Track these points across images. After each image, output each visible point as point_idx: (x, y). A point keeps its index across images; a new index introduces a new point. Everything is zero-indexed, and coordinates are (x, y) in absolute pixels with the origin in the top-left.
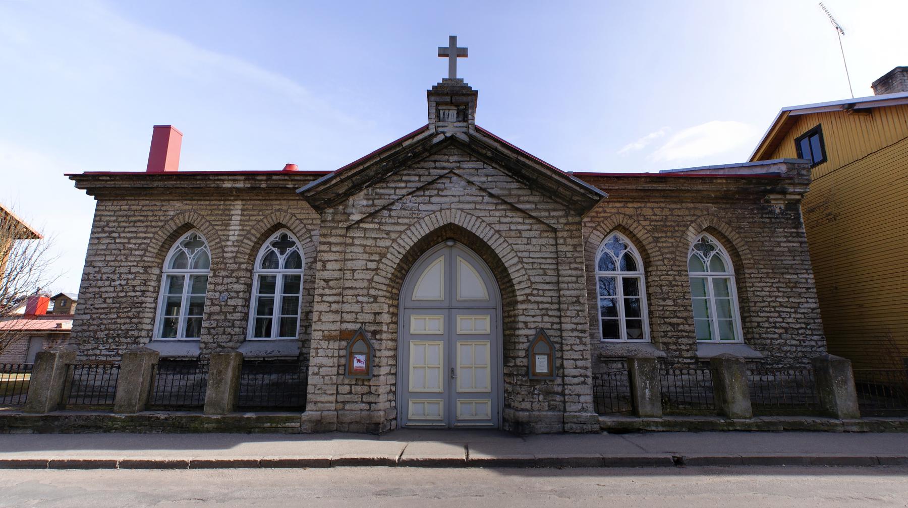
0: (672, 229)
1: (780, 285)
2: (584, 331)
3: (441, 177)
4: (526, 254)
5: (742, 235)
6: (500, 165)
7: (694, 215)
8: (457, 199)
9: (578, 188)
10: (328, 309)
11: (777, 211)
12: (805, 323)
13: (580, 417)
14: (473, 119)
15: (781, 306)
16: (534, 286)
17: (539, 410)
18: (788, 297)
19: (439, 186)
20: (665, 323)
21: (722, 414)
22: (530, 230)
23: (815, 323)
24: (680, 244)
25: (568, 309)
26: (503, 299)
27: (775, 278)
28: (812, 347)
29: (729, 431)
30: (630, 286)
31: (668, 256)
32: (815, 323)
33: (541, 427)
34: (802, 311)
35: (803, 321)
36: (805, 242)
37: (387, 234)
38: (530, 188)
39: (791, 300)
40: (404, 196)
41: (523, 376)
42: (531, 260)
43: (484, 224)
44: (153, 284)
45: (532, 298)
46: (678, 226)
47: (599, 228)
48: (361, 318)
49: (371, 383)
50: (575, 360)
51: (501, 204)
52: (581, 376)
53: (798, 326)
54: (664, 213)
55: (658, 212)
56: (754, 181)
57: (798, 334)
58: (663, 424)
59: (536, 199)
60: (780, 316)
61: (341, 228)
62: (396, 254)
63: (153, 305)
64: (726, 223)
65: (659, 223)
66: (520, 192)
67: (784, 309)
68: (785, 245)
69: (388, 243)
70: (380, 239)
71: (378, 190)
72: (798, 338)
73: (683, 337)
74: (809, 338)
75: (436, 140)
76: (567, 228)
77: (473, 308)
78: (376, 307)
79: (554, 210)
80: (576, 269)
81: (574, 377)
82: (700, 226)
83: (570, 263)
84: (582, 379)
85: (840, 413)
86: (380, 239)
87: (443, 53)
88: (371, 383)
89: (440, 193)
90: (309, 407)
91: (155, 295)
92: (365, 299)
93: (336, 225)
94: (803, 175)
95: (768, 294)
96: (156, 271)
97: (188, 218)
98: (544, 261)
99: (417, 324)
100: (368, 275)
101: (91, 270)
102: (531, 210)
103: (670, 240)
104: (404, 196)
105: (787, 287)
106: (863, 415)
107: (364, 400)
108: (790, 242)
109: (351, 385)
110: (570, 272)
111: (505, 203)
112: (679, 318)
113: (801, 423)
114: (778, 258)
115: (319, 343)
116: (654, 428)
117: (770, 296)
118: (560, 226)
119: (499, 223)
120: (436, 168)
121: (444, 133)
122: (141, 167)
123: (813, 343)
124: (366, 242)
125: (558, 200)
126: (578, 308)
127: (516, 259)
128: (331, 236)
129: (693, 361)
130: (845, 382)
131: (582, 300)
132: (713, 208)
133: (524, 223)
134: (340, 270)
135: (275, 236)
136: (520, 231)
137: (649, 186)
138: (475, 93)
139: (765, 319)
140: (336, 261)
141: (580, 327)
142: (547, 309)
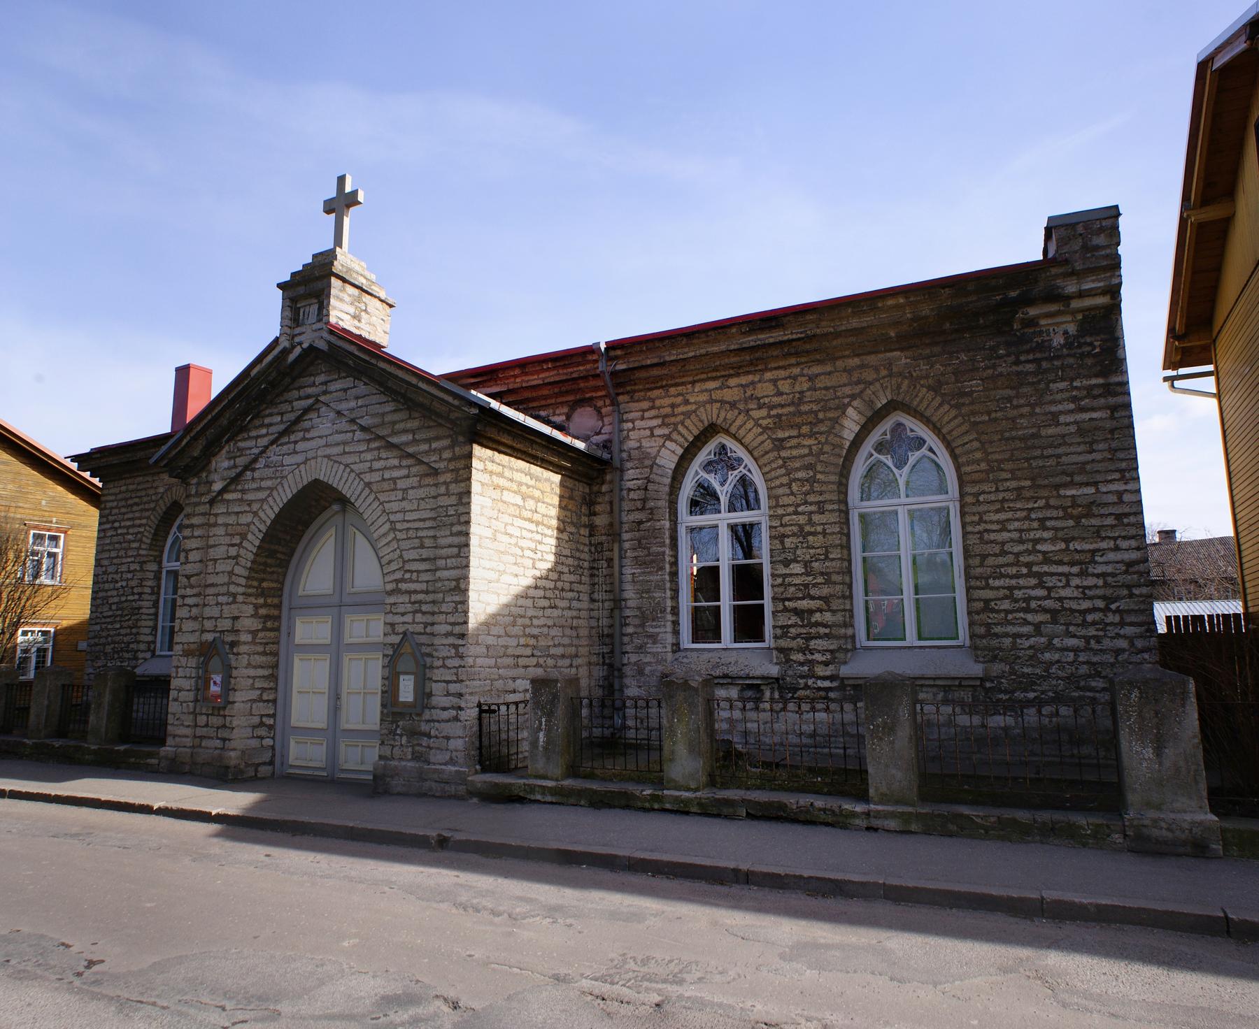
0: (811, 418)
1: (1048, 513)
3: (307, 410)
4: (399, 516)
5: (964, 410)
7: (858, 383)
8: (323, 442)
9: (450, 399)
11: (1058, 340)
12: (1104, 598)
13: (443, 771)
15: (1047, 560)
16: (407, 567)
20: (786, 610)
21: (660, 782)
22: (408, 476)
23: (1131, 595)
24: (827, 448)
25: (444, 601)
27: (1036, 499)
28: (1118, 652)
29: (654, 810)
30: (744, 536)
31: (801, 475)
32: (1131, 595)
33: (397, 784)
34: (1100, 569)
35: (1099, 592)
37: (249, 505)
40: (267, 447)
42: (406, 525)
43: (353, 475)
44: (150, 583)
45: (403, 586)
46: (824, 409)
47: (675, 436)
50: (448, 682)
51: (374, 439)
52: (453, 708)
53: (1086, 605)
54: (798, 388)
55: (785, 386)
56: (971, 287)
57: (1084, 624)
58: (553, 791)
59: (414, 424)
60: (1041, 585)
63: (968, 519)
64: (929, 388)
65: (785, 410)
66: (396, 417)
67: (1054, 569)
68: (1070, 419)
71: (241, 444)
72: (1083, 632)
73: (819, 637)
74: (1112, 631)
75: (292, 357)
78: (234, 610)
79: (437, 438)
81: (444, 709)
83: (452, 525)
84: (454, 713)
85: (872, 792)
87: (329, 207)
90: (170, 741)
91: (154, 597)
94: (1097, 248)
95: (1015, 535)
96: (154, 567)
98: (421, 525)
99: (309, 629)
101: (100, 570)
102: (407, 444)
103: (807, 442)
104: (267, 447)
105: (1067, 516)
106: (924, 798)
108: (1082, 410)
109: (208, 715)
110: (450, 540)
112: (813, 598)
113: (782, 806)
114: (1050, 451)
116: (539, 797)
117: (1021, 541)
118: (442, 465)
119: (371, 470)
120: (300, 398)
121: (300, 344)
122: (1041, 258)
123: (1123, 644)
126: (457, 598)
127: (387, 526)
129: (835, 684)
130: (891, 729)
132: (901, 359)
133: (400, 467)
136: (394, 480)
137: (750, 340)
139: (1002, 593)
142: (420, 602)
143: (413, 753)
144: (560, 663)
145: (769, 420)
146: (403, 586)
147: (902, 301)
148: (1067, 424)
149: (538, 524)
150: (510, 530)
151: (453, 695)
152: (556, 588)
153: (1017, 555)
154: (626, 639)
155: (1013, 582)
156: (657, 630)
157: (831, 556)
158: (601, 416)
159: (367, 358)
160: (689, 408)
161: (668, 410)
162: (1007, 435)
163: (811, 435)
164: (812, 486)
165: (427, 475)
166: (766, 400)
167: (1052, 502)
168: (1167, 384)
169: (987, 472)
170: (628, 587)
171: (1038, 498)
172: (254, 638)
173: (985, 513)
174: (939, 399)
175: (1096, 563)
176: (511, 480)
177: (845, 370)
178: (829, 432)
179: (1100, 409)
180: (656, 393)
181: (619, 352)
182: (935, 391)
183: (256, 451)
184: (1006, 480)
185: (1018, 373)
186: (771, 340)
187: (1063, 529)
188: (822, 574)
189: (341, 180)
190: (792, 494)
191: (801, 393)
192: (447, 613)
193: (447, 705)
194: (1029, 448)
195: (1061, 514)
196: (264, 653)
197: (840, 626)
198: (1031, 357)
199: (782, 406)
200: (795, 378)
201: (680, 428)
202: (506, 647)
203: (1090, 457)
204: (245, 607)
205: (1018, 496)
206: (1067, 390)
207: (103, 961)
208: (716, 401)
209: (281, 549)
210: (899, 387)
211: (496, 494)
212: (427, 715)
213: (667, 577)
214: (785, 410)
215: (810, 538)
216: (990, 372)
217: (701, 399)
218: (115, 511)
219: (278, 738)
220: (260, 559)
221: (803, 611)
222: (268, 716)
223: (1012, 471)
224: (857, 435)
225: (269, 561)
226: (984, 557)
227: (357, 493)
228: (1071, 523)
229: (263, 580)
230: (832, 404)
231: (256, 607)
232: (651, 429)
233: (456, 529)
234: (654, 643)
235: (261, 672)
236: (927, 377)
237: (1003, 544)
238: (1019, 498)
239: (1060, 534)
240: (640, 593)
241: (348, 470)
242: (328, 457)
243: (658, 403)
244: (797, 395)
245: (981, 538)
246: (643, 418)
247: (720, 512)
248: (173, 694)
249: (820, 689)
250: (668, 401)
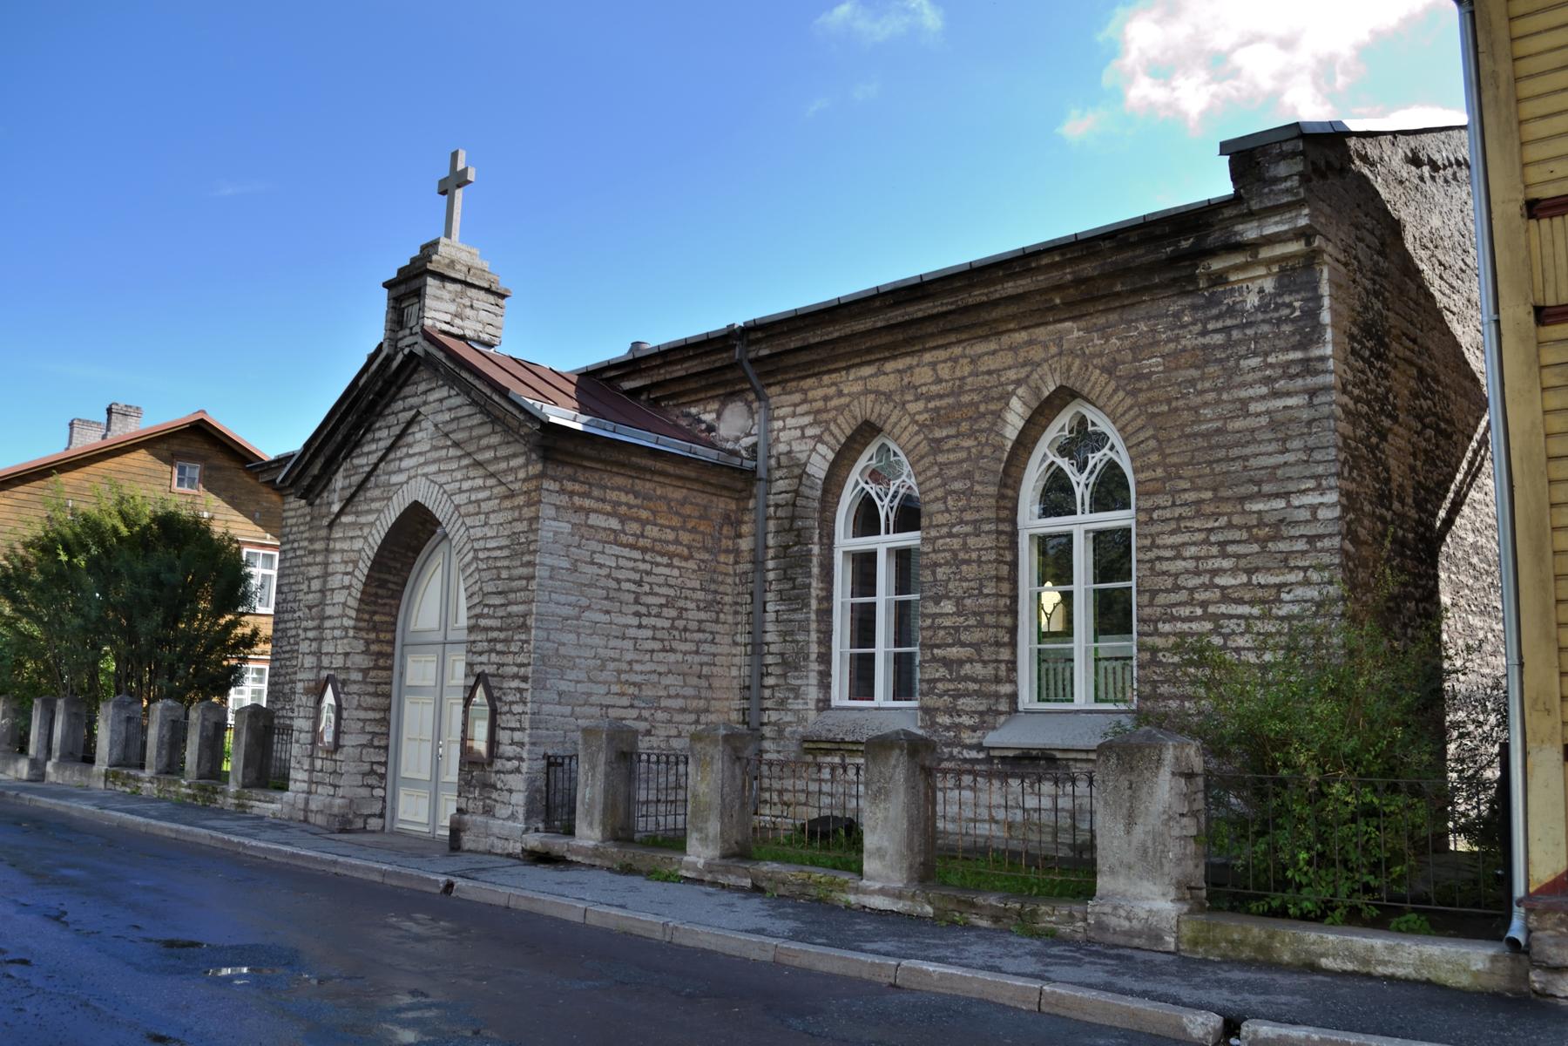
3: (410, 423)
4: (481, 544)
5: (1142, 397)
7: (1024, 365)
9: (516, 412)
11: (1253, 300)
15: (1226, 598)
18: (1250, 572)
20: (934, 659)
31: (958, 486)
36: (1326, 389)
39: (1259, 578)
42: (487, 554)
47: (826, 437)
50: (513, 729)
54: (958, 374)
55: (944, 371)
63: (1007, 621)
64: (1103, 369)
65: (944, 402)
73: (967, 694)
75: (395, 364)
79: (515, 456)
95: (1191, 565)
97: (866, 408)
105: (1253, 539)
108: (1276, 394)
112: (963, 645)
114: (1235, 452)
117: (1197, 573)
118: (516, 486)
119: (461, 491)
120: (404, 410)
126: (523, 637)
129: (982, 755)
133: (484, 488)
135: (1060, 426)
137: (897, 315)
142: (495, 640)
144: (677, 718)
145: (926, 416)
147: (1057, 259)
148: (1258, 415)
149: (644, 550)
150: (599, 559)
152: (673, 627)
153: (1192, 590)
154: (767, 693)
155: (1185, 626)
156: (799, 682)
157: (986, 591)
158: (752, 413)
160: (843, 400)
161: (820, 404)
162: (1188, 430)
163: (972, 434)
164: (968, 500)
166: (924, 389)
167: (1236, 520)
169: (1163, 480)
170: (770, 627)
171: (1220, 514)
172: (365, 677)
173: (1158, 534)
174: (1113, 384)
175: (1281, 601)
176: (603, 501)
178: (990, 430)
179: (1296, 393)
180: (810, 382)
181: (760, 335)
182: (1110, 374)
183: (367, 469)
184: (1185, 490)
185: (1205, 347)
186: (920, 314)
187: (1246, 556)
188: (974, 614)
189: (455, 156)
190: (948, 511)
191: (962, 379)
193: (511, 755)
194: (1211, 448)
195: (1245, 536)
196: (376, 695)
197: (990, 681)
198: (1220, 325)
199: (941, 397)
200: (955, 360)
201: (833, 427)
202: (590, 694)
203: (1281, 459)
204: (355, 642)
205: (1197, 512)
206: (1260, 369)
207: (149, 1036)
208: (871, 392)
209: (391, 578)
210: (1069, 369)
211: (578, 518)
212: (498, 764)
213: (813, 616)
214: (944, 402)
215: (964, 567)
216: (1172, 346)
217: (855, 389)
218: (295, 529)
219: (389, 788)
220: (369, 590)
221: (952, 662)
222: (379, 763)
223: (1191, 479)
224: (1021, 432)
225: (380, 592)
226: (1154, 593)
228: (1256, 548)
229: (375, 613)
230: (995, 393)
231: (368, 643)
232: (802, 428)
233: (526, 558)
234: (796, 698)
235: (371, 715)
236: (1101, 355)
237: (1177, 576)
238: (1199, 514)
239: (1243, 563)
240: (784, 635)
242: (425, 475)
243: (810, 395)
245: (1152, 569)
246: (794, 415)
247: (1074, 513)
248: (295, 734)
249: (965, 760)
250: (820, 393)
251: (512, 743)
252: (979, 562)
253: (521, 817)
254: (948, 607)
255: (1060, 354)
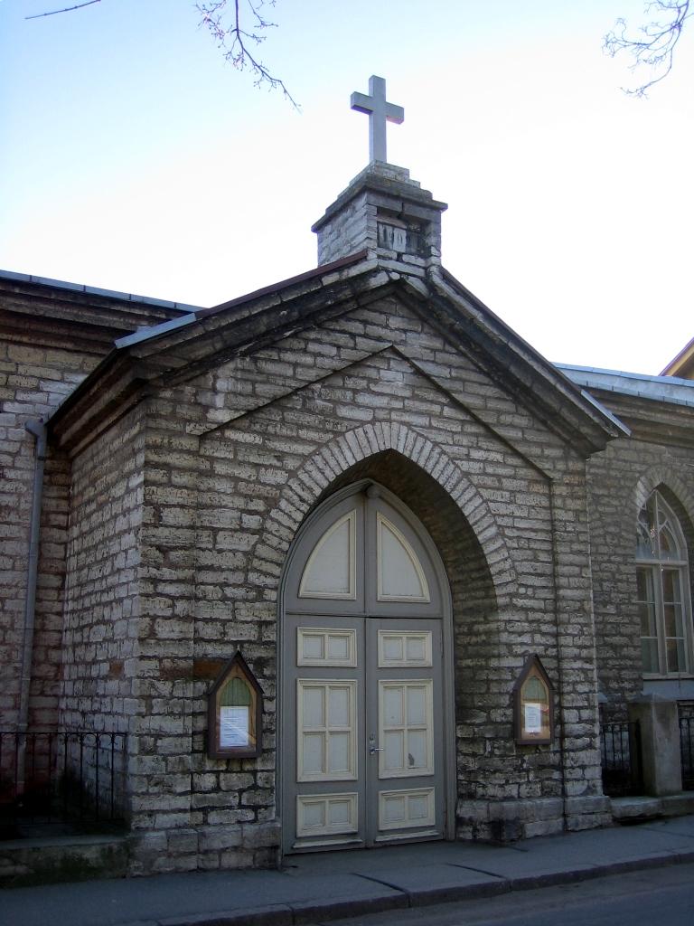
2: (588, 660)
3: (375, 355)
6: (471, 350)
10: (168, 613)
14: (439, 257)
16: (524, 580)
17: (529, 798)
19: (372, 373)
25: (569, 623)
26: (454, 601)
31: (612, 529)
37: (278, 458)
38: (516, 401)
41: (507, 740)
42: (517, 533)
43: (445, 459)
48: (233, 635)
49: (259, 766)
50: (579, 708)
52: (586, 735)
61: (190, 435)
62: (298, 503)
64: (681, 480)
69: (280, 477)
70: (267, 467)
73: (625, 668)
76: (567, 479)
77: (405, 616)
79: (549, 445)
80: (580, 552)
82: (651, 481)
83: (572, 542)
86: (267, 467)
88: (259, 766)
89: (373, 387)
92: (240, 592)
93: (178, 427)
98: (532, 535)
100: (245, 541)
102: (517, 441)
103: (615, 503)
107: (244, 802)
109: (217, 773)
110: (571, 558)
111: (477, 421)
112: (622, 635)
115: (152, 685)
119: (468, 458)
120: (366, 336)
124: (237, 472)
125: (556, 429)
126: (581, 620)
128: (171, 450)
131: (586, 607)
132: (667, 453)
133: (505, 465)
134: (192, 527)
136: (499, 477)
138: (402, 109)
140: (182, 506)
141: (585, 653)
142: (538, 621)
143: (542, 790)
146: (520, 602)
151: (586, 721)
159: (87, 416)
163: (618, 497)
165: (537, 482)
168: (391, 98)
177: (635, 450)
181: (640, 404)
188: (628, 615)
192: (574, 636)
199: (599, 467)
210: (666, 474)
221: (616, 646)
227: (453, 481)
241: (437, 450)
244: (608, 462)
251: (580, 721)
252: (628, 582)
253: (599, 789)
254: (611, 609)
255: (661, 463)
